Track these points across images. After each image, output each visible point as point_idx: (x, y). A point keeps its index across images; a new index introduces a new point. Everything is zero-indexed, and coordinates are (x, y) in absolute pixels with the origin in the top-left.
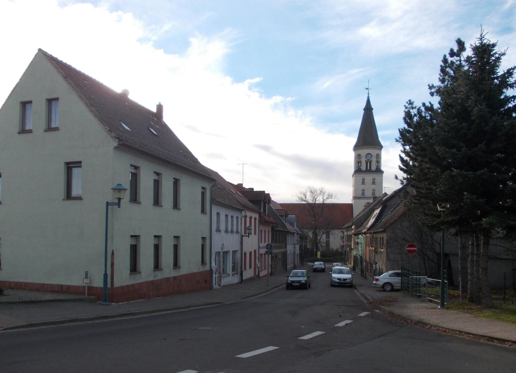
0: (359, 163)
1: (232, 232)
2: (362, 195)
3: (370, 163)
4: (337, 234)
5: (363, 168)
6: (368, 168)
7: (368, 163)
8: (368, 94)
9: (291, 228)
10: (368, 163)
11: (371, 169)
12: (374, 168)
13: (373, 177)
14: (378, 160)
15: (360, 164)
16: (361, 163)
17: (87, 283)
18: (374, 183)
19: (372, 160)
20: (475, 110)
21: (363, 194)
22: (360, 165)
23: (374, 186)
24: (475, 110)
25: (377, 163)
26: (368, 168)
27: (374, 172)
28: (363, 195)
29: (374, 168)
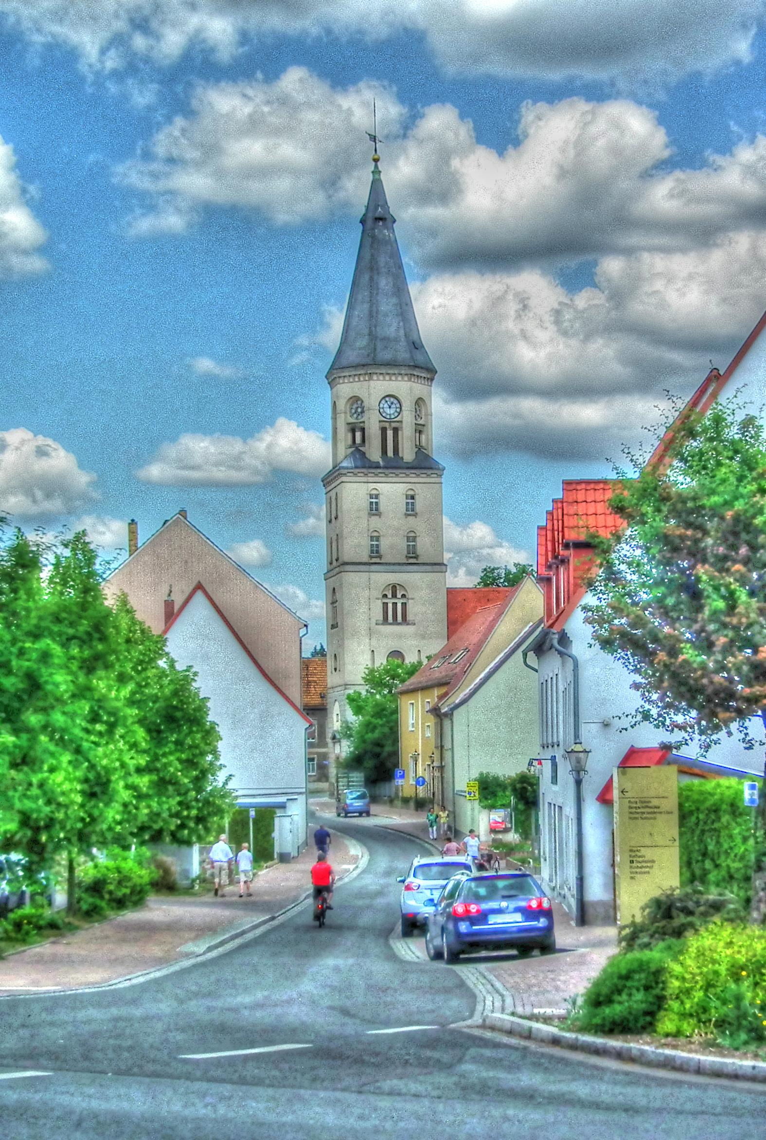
0: (353, 431)
1: (395, 621)
2: (371, 557)
3: (396, 431)
4: (29, 793)
5: (375, 455)
6: (390, 453)
7: (390, 433)
8: (376, 161)
9: (152, 976)
10: (390, 433)
11: (400, 455)
12: (408, 454)
13: (410, 486)
14: (421, 422)
15: (358, 435)
16: (363, 430)
17: (255, 1099)
18: (411, 510)
19: (401, 422)
20: (565, 324)
21: (375, 551)
22: (358, 440)
23: (375, 522)
24: (565, 324)
25: (418, 435)
26: (390, 453)
27: (410, 467)
28: (376, 557)
29: (408, 454)
